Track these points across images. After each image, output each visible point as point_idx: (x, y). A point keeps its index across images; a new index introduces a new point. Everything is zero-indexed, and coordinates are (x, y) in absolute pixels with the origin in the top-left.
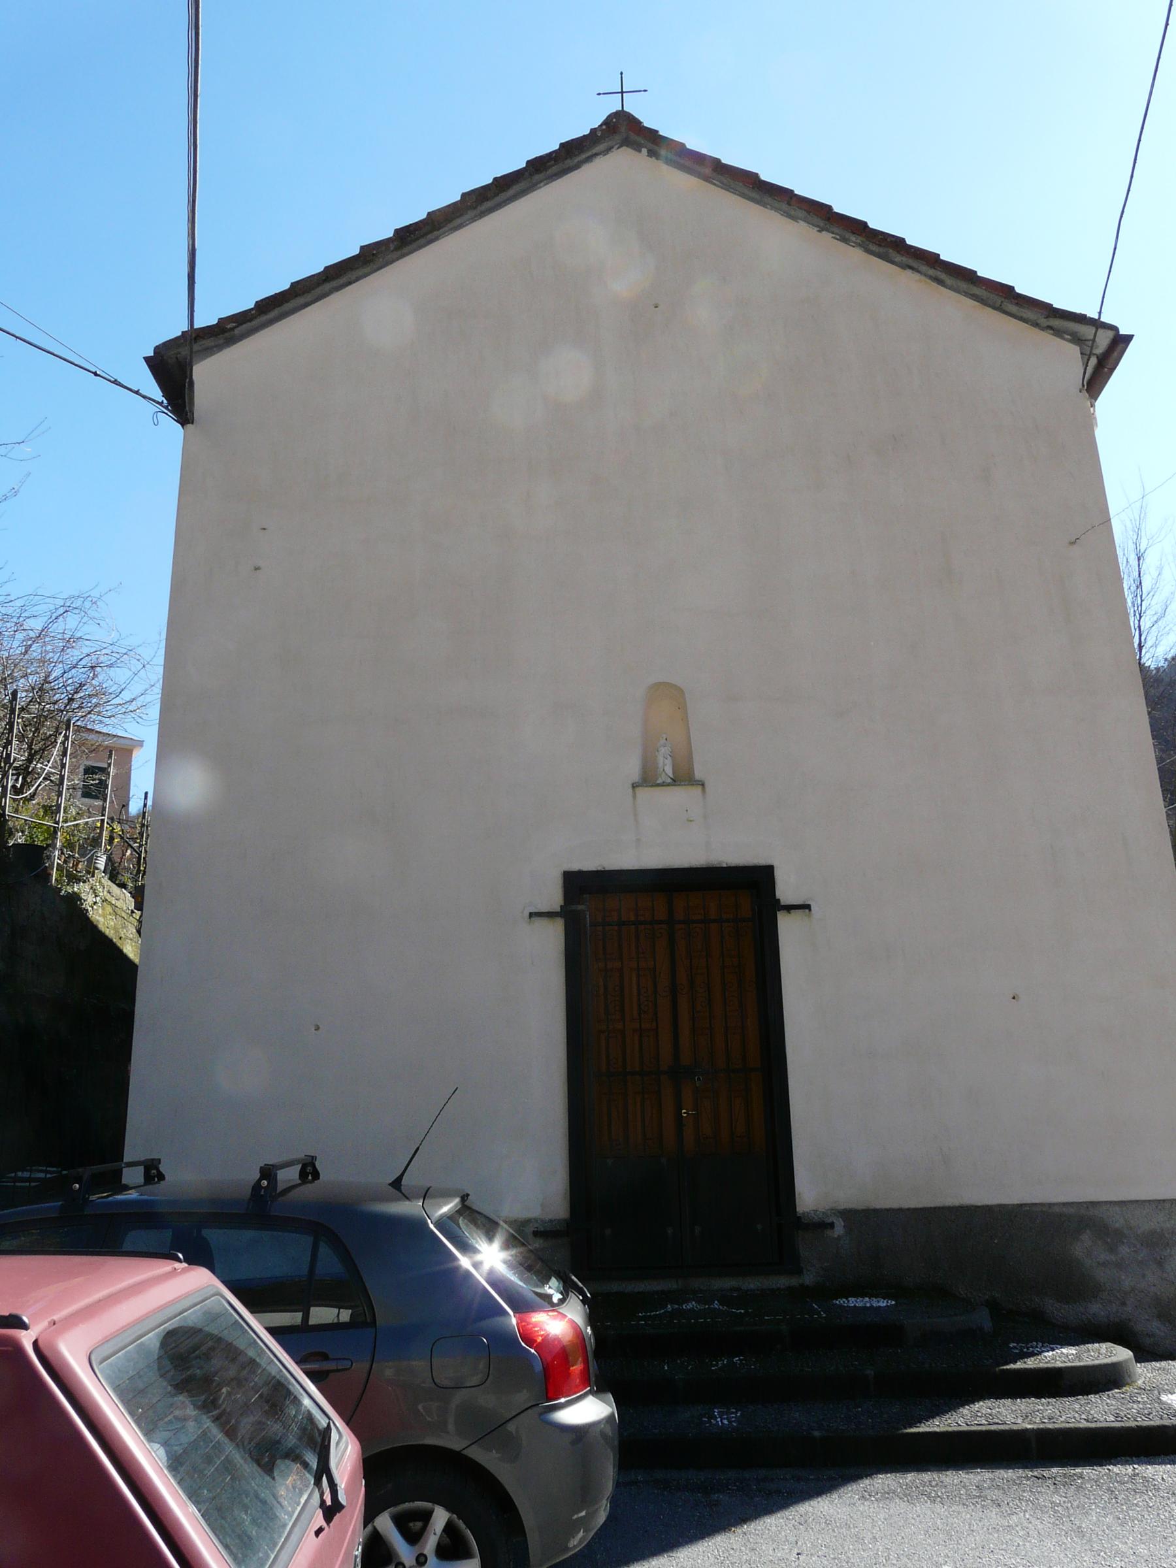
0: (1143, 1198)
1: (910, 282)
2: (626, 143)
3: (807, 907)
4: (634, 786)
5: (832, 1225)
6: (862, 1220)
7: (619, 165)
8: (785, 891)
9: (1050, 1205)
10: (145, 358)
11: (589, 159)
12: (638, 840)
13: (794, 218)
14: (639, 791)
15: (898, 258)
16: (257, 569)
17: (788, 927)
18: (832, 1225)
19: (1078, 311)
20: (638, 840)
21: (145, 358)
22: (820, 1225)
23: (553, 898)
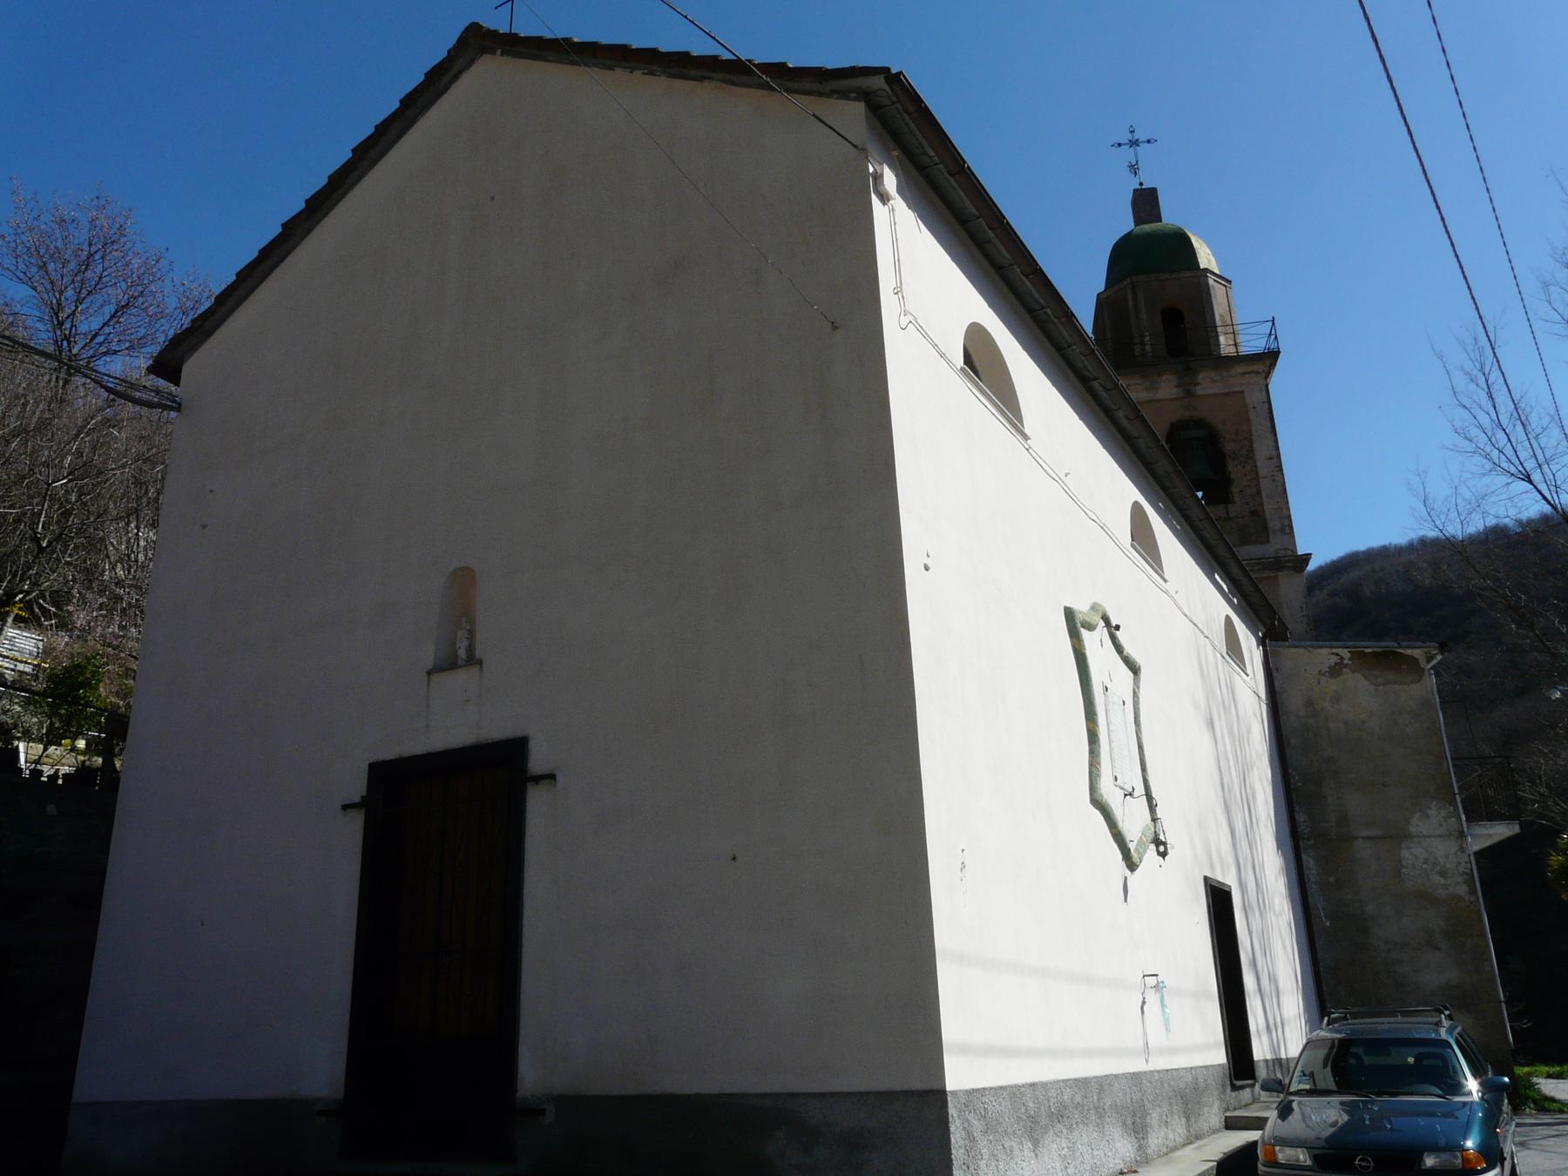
0: (845, 1089)
1: (742, 103)
2: (484, 51)
3: (551, 777)
4: (429, 673)
5: (543, 1112)
6: (574, 1106)
7: (487, 71)
8: (537, 762)
9: (748, 1095)
10: (1206, 879)
11: (456, 77)
12: (428, 726)
13: (611, 68)
14: (435, 678)
15: (693, 73)
16: (204, 526)
17: (537, 802)
18: (543, 1112)
19: (846, 65)
20: (428, 726)
21: (1206, 879)
22: (534, 1111)
23: (356, 787)
